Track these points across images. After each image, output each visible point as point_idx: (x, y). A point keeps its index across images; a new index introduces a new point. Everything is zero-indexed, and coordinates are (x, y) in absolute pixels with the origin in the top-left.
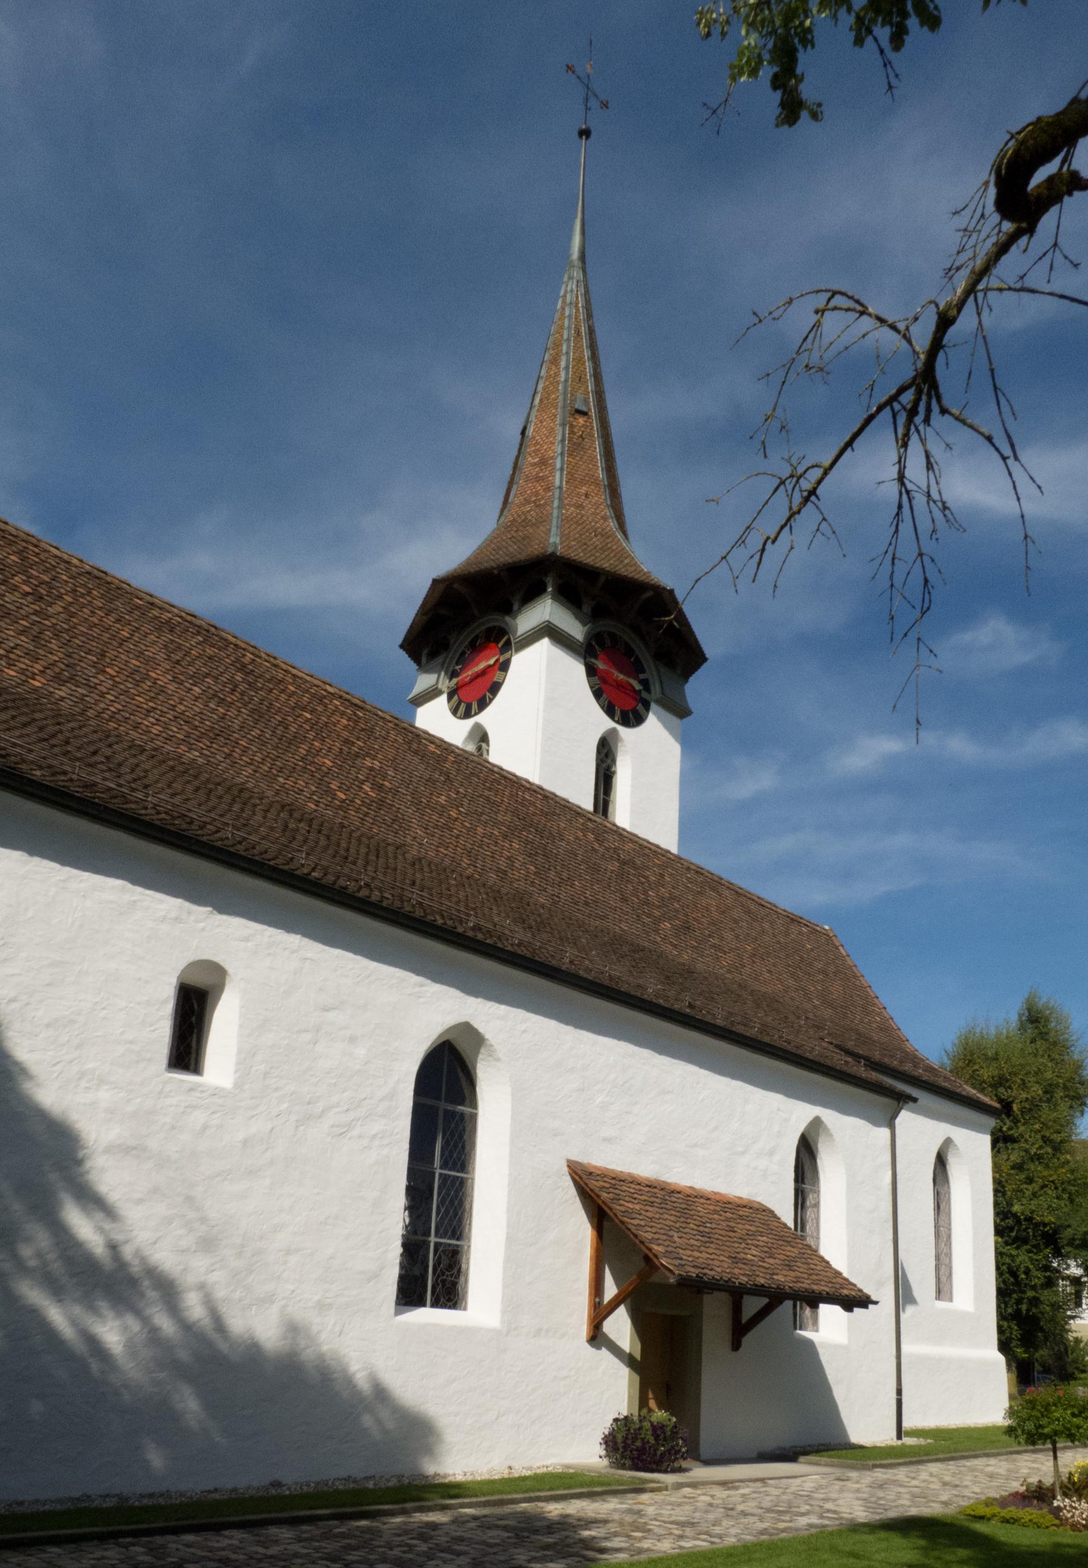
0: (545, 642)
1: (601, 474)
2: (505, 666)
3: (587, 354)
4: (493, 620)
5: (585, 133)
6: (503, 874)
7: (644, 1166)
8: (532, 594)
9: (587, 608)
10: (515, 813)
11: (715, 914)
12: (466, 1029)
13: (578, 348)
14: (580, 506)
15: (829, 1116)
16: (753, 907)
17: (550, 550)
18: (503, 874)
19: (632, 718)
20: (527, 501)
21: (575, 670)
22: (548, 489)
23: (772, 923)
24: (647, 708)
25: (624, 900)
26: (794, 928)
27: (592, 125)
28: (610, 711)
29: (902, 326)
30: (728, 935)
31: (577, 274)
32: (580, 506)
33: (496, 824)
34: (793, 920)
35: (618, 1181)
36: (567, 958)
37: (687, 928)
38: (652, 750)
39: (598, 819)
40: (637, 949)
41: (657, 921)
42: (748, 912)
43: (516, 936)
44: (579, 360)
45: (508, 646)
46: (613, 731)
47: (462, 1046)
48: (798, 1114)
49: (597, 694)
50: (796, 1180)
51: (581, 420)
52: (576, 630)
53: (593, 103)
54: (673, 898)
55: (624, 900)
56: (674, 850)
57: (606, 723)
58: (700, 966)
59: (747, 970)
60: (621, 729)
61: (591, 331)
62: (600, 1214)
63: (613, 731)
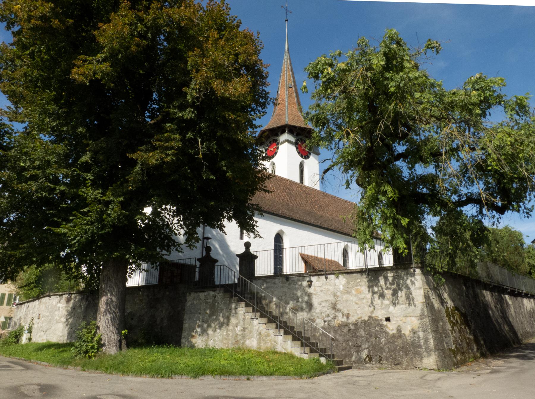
0: (286, 143)
1: (296, 101)
2: (278, 148)
3: (291, 73)
4: (275, 138)
5: (287, 20)
6: (283, 200)
7: (306, 253)
8: (283, 132)
9: (295, 134)
10: (284, 186)
11: (327, 203)
12: (281, 231)
13: (289, 72)
14: (292, 110)
15: (349, 244)
16: (336, 200)
17: (286, 123)
18: (283, 200)
19: (307, 157)
20: (280, 109)
21: (293, 148)
22: (284, 106)
23: (341, 203)
24: (310, 154)
25: (307, 202)
26: (346, 204)
27: (288, 18)
28: (302, 156)
29: (332, 164)
30: (330, 207)
31: (287, 54)
32: (292, 110)
33: (281, 189)
34: (346, 202)
35: (305, 255)
36: (297, 217)
37: (321, 207)
38: (312, 165)
39: (301, 184)
40: (310, 212)
41: (314, 206)
42: (335, 201)
43: (288, 214)
44: (289, 75)
45: (278, 144)
46: (303, 161)
47: (281, 234)
48: (343, 245)
49: (299, 153)
50: (343, 256)
51: (291, 89)
52: (293, 139)
53: (288, 13)
54: (318, 200)
55: (307, 202)
56: (318, 187)
57: (300, 159)
58: (324, 215)
59: (334, 215)
60: (305, 160)
61: (291, 67)
62: (306, 262)
63: (303, 161)
